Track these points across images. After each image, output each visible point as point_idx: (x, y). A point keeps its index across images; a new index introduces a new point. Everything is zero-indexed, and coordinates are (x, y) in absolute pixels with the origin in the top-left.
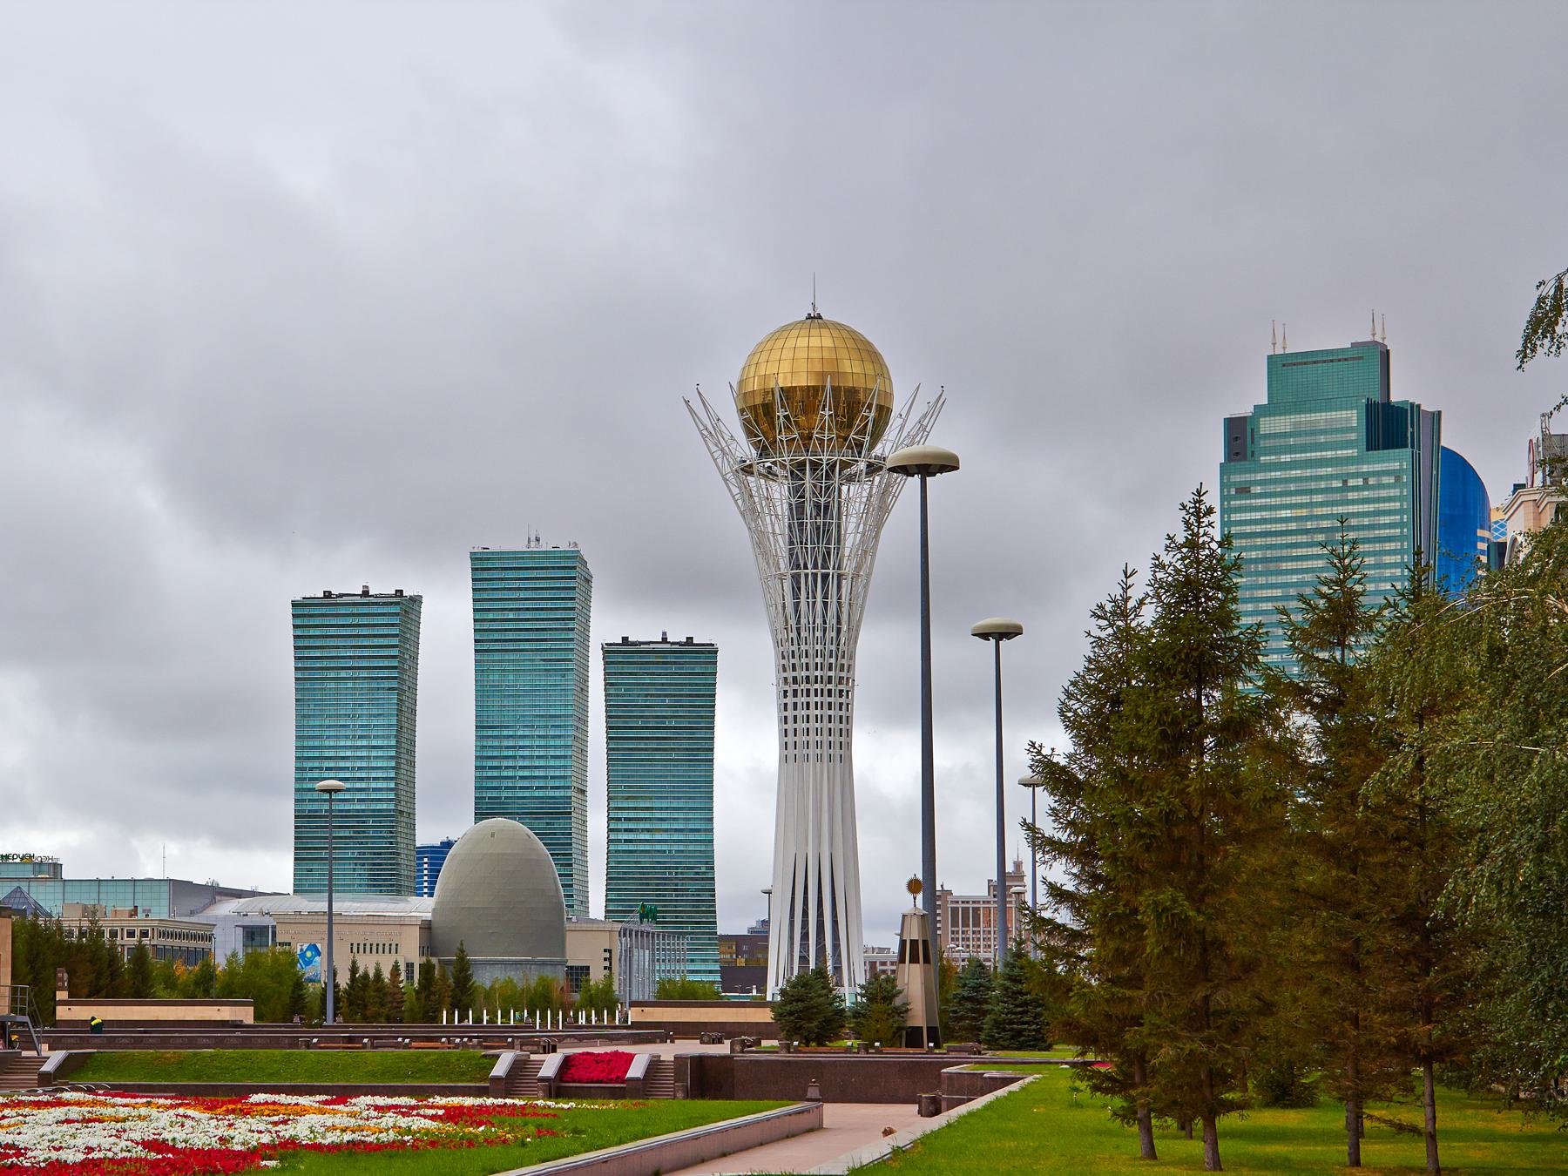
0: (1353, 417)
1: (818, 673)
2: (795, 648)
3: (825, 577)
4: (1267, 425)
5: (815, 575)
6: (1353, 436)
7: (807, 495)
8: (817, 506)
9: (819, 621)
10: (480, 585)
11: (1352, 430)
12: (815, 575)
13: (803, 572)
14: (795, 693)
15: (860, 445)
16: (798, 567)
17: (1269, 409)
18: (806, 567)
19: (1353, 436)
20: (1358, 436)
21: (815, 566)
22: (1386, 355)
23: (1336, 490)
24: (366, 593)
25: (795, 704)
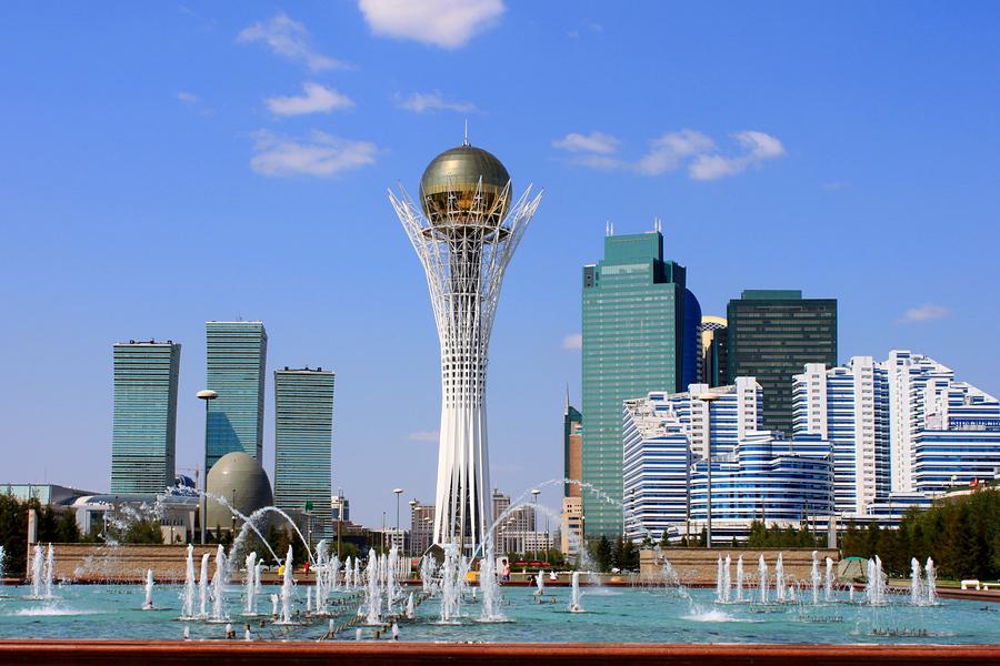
0: (647, 267)
1: (468, 355)
2: (454, 339)
3: (473, 298)
4: (606, 270)
5: (467, 297)
6: (647, 276)
7: (464, 247)
8: (470, 255)
9: (469, 324)
10: (280, 388)
11: (646, 273)
12: (467, 297)
13: (460, 295)
14: (454, 367)
15: (496, 218)
16: (456, 291)
17: (602, 263)
18: (462, 291)
19: (647, 276)
20: (650, 276)
21: (467, 291)
22: (264, 339)
23: (640, 302)
24: (319, 370)
25: (454, 374)
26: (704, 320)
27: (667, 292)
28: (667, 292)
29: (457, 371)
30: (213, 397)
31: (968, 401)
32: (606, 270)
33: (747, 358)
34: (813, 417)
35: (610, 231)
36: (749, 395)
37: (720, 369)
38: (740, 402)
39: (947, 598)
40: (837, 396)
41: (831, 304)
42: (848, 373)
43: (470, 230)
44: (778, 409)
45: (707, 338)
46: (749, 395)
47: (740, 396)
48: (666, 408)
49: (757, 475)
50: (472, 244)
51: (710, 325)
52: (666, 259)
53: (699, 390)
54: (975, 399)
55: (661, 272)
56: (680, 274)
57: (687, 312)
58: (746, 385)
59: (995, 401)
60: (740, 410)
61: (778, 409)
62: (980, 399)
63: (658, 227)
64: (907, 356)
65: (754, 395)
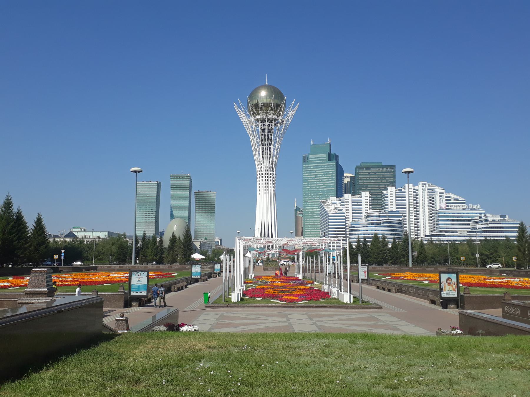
0: (325, 155)
3: (270, 148)
4: (310, 156)
22: (191, 181)
26: (345, 175)
27: (333, 163)
28: (333, 163)
29: (263, 172)
30: (139, 172)
31: (453, 199)
32: (310, 156)
33: (363, 186)
34: (391, 204)
35: (312, 142)
36: (366, 198)
37: (354, 188)
38: (363, 201)
39: (476, 274)
40: (400, 197)
41: (393, 167)
42: (403, 190)
43: (268, 120)
44: (378, 202)
45: (346, 180)
46: (366, 198)
47: (363, 198)
48: (336, 203)
49: (375, 227)
50: (269, 125)
51: (347, 177)
52: (332, 152)
53: (348, 197)
54: (455, 199)
55: (330, 157)
56: (337, 157)
57: (339, 172)
58: (365, 195)
59: (462, 199)
60: (363, 204)
61: (378, 202)
62: (457, 199)
63: (329, 141)
64: (425, 184)
65: (368, 198)
